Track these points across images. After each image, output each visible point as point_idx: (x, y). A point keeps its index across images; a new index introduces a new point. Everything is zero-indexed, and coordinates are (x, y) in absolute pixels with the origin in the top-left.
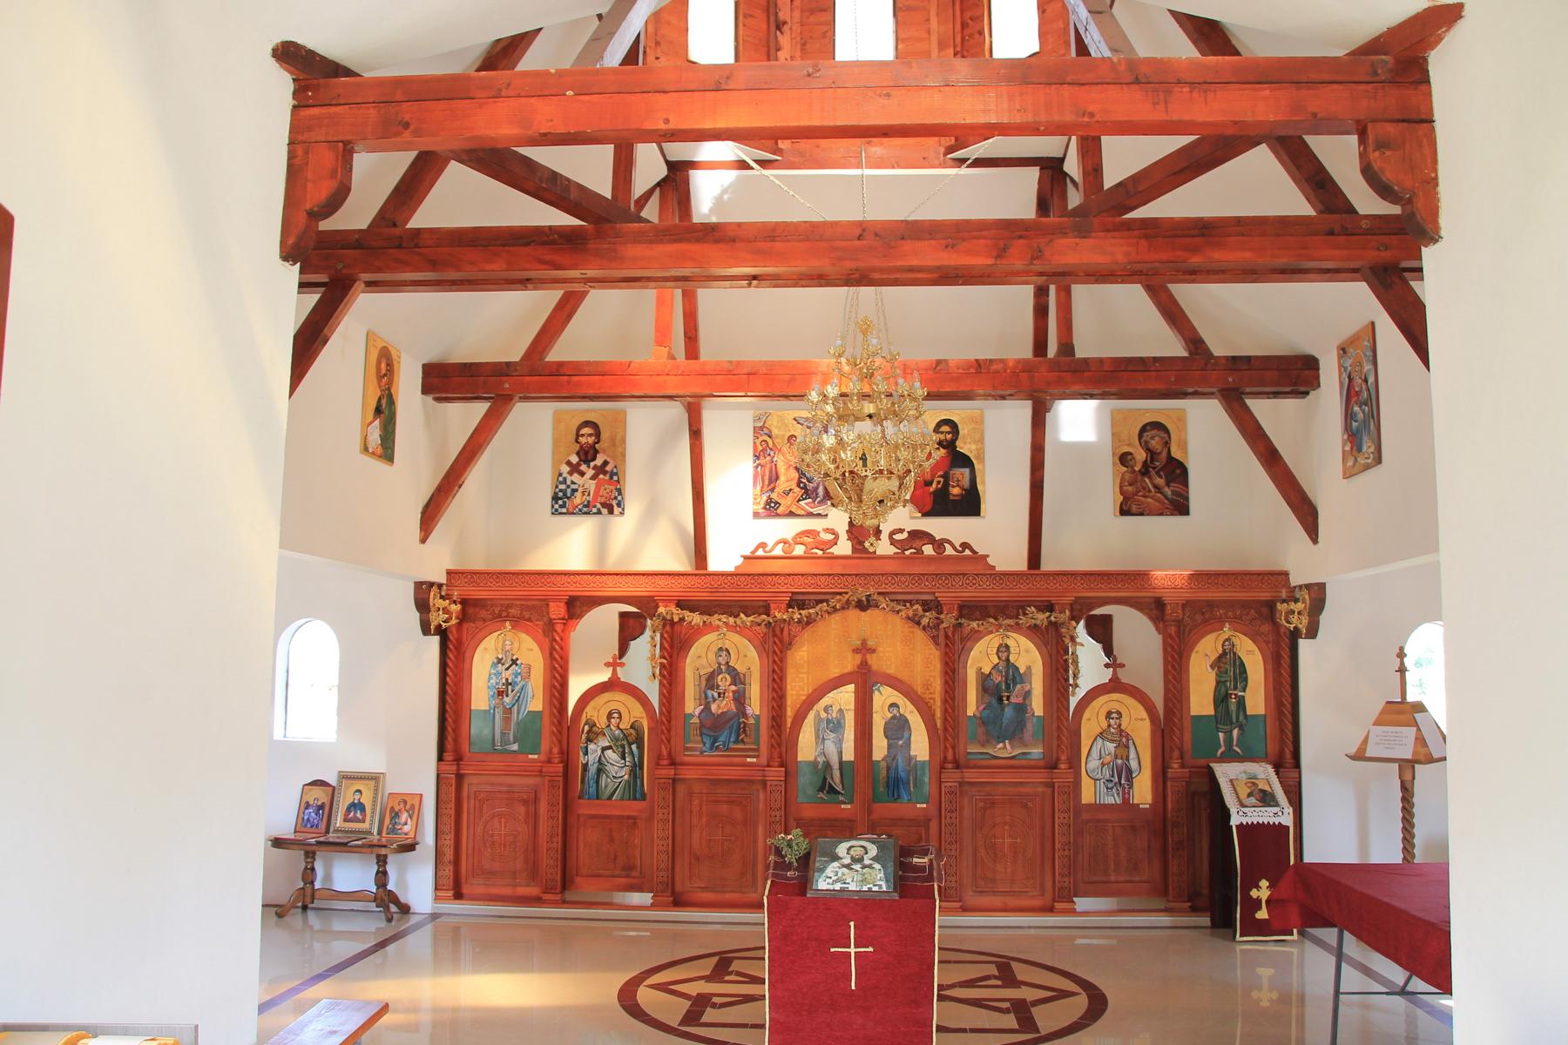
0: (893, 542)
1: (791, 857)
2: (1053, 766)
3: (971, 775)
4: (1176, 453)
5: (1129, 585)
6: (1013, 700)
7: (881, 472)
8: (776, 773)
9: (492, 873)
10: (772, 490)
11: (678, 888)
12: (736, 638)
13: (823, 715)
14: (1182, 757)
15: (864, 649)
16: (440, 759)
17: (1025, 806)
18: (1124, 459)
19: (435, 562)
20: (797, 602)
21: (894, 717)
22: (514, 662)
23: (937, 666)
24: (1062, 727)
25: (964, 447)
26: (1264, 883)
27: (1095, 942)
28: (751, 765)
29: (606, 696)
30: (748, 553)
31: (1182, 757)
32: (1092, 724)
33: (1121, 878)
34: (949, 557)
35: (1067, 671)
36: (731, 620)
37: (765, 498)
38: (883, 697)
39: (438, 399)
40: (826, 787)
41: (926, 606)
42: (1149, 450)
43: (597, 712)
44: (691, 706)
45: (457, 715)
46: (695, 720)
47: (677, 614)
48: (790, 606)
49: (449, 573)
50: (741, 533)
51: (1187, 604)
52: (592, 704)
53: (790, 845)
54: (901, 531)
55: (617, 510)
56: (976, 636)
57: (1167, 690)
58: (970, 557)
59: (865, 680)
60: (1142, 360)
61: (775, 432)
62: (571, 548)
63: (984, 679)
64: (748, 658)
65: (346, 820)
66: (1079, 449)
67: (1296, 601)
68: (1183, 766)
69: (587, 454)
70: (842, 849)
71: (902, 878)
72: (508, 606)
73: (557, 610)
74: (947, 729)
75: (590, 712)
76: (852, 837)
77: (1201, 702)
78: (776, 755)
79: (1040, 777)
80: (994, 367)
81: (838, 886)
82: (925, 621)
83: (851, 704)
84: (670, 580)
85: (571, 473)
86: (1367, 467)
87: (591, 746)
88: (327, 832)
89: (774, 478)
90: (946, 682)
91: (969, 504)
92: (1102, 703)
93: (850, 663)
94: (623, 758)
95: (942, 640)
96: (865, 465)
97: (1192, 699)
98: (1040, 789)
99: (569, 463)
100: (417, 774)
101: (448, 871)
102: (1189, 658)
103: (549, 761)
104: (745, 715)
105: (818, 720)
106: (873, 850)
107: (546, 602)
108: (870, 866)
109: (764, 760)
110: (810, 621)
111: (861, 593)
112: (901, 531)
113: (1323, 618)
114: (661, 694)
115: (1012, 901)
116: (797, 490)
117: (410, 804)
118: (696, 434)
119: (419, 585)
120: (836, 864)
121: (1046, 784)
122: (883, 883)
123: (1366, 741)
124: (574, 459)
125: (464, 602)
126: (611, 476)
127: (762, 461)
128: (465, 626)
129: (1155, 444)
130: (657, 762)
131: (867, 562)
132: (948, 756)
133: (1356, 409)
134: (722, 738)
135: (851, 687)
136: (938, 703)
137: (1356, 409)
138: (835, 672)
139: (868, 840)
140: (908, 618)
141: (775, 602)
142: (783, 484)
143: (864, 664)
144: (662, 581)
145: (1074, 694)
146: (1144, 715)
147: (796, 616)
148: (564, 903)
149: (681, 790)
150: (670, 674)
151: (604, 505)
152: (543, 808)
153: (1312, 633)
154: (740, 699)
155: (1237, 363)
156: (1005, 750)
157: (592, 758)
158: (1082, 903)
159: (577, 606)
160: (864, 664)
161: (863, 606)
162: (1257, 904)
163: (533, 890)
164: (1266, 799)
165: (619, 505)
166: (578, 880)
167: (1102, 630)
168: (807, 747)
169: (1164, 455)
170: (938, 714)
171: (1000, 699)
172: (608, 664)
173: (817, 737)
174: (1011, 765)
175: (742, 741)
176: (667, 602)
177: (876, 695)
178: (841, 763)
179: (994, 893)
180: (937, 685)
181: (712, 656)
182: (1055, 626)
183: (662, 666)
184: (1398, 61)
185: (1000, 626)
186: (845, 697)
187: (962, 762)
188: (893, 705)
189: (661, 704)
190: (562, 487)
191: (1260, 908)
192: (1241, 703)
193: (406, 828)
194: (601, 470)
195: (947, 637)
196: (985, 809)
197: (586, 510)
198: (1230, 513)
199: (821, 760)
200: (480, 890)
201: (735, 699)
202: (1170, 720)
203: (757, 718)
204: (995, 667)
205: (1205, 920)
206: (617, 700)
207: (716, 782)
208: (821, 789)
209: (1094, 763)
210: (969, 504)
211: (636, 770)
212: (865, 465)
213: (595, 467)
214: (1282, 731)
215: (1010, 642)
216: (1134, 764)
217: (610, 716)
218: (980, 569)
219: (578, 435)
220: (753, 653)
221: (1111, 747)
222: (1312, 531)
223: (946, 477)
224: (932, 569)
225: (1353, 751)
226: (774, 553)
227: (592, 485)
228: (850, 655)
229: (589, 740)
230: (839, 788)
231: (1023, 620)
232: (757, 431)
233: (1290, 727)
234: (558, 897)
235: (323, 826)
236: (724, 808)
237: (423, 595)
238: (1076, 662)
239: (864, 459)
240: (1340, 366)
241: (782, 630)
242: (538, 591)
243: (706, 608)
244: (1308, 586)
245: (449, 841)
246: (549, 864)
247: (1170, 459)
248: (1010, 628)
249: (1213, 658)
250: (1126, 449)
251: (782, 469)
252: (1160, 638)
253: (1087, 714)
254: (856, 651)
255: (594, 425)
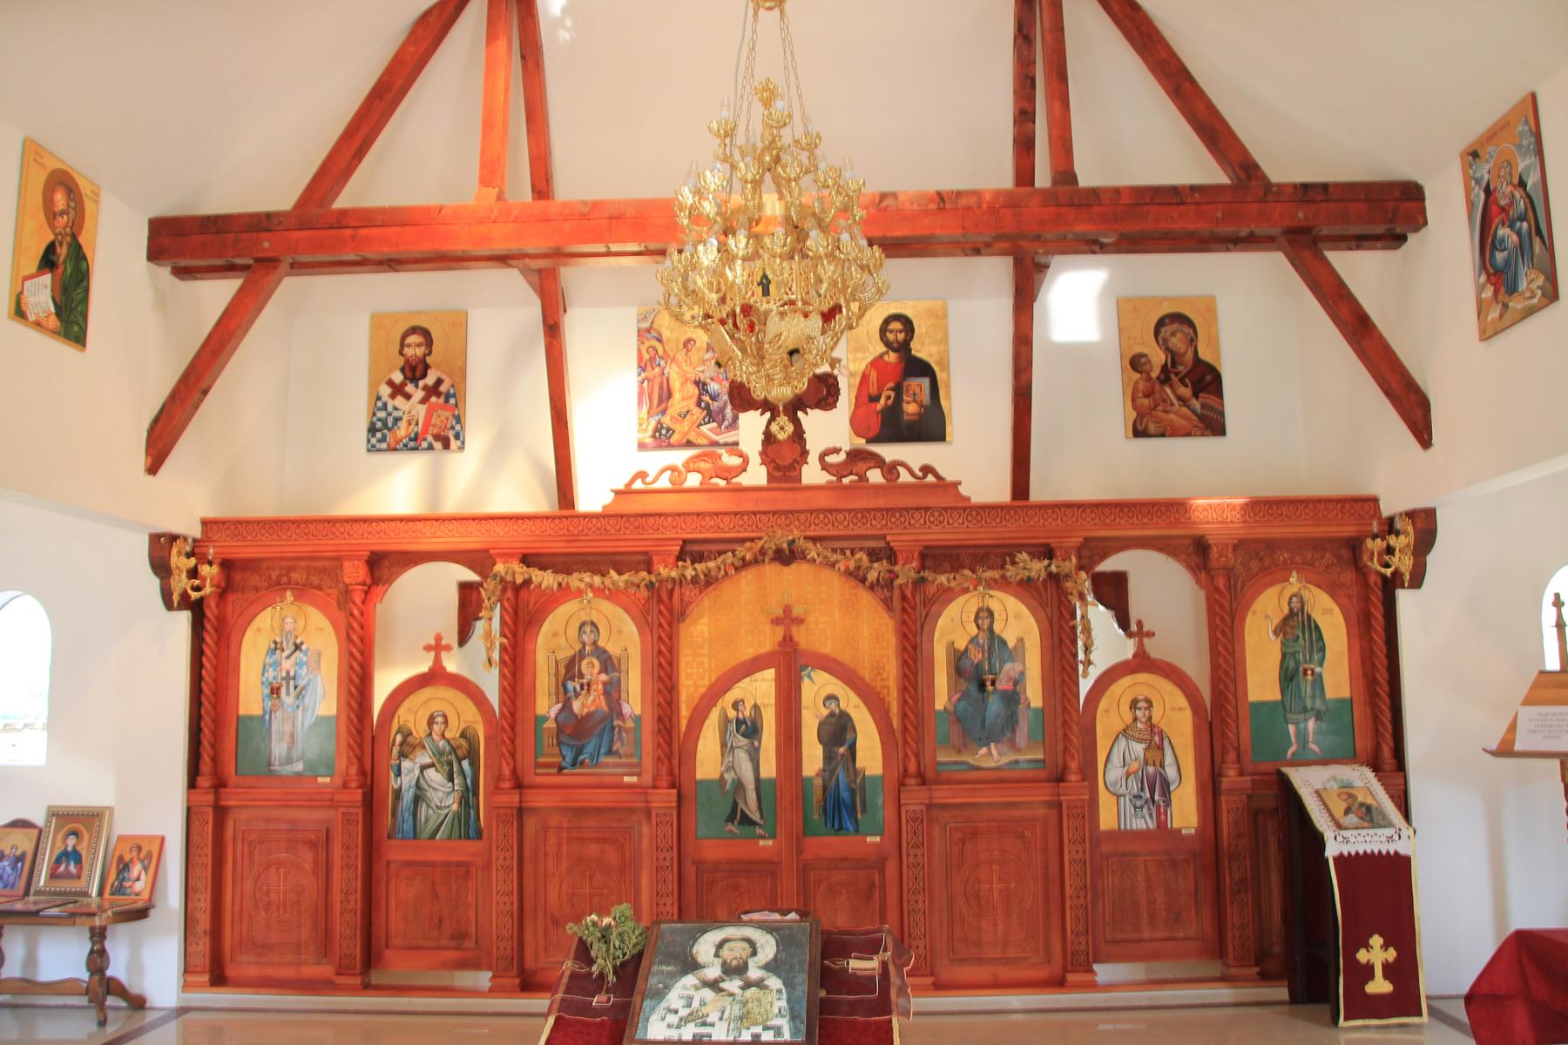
0: (825, 467)
1: (603, 964)
2: (1060, 778)
3: (942, 795)
4: (1205, 354)
5: (1160, 522)
6: (998, 685)
7: (793, 303)
8: (664, 798)
9: (266, 947)
10: (664, 412)
11: (530, 963)
12: (607, 607)
13: (732, 714)
14: (1239, 760)
15: (787, 619)
16: (192, 784)
17: (1021, 836)
18: (1136, 363)
19: (184, 500)
20: (690, 552)
21: (832, 714)
22: (297, 647)
23: (890, 641)
24: (1070, 725)
25: (921, 349)
26: (1376, 941)
27: (1126, 1027)
28: (630, 786)
29: (427, 693)
30: (621, 487)
31: (1239, 761)
32: (1110, 718)
33: (1158, 935)
34: (905, 486)
35: (1074, 642)
36: (597, 580)
37: (653, 423)
38: (817, 687)
39: (182, 272)
40: (737, 816)
41: (874, 555)
42: (1168, 350)
43: (412, 715)
44: (546, 706)
45: (218, 722)
46: (551, 724)
47: (520, 572)
48: (680, 557)
49: (205, 523)
50: (617, 455)
51: (1240, 545)
52: (406, 704)
53: (605, 938)
54: (836, 451)
55: (454, 444)
56: (946, 595)
57: (1215, 668)
58: (937, 486)
59: (790, 663)
60: (1174, 190)
61: (666, 334)
62: (396, 489)
63: (958, 660)
64: (624, 635)
65: (53, 875)
66: (1076, 353)
67: (1397, 534)
68: (1241, 773)
69: (415, 371)
70: (704, 947)
71: (825, 1006)
72: (290, 569)
73: (355, 572)
74: (908, 726)
75: (404, 715)
76: (719, 923)
77: (1262, 684)
78: (664, 771)
79: (1042, 794)
80: (964, 201)
81: (688, 1033)
82: (872, 576)
83: (776, 682)
84: (514, 527)
85: (393, 396)
86: (1530, 312)
87: (406, 764)
88: (27, 893)
89: (666, 395)
90: (905, 662)
91: (930, 427)
92: (1123, 688)
93: (767, 640)
94: (451, 779)
95: (897, 603)
96: (766, 292)
97: (1250, 678)
98: (1041, 812)
99: (390, 383)
100: (156, 807)
101: (203, 946)
102: (1243, 620)
103: (345, 786)
104: (621, 715)
105: (725, 721)
106: (768, 947)
107: (338, 559)
108: (759, 984)
109: (648, 779)
110: (709, 581)
111: (782, 539)
112: (836, 451)
113: (1431, 559)
114: (503, 689)
115: (1006, 973)
116: (696, 411)
117: (148, 851)
118: (553, 331)
119: (155, 539)
120: (690, 980)
121: (1050, 805)
122: (784, 1023)
123: (1513, 728)
124: (398, 377)
125: (227, 565)
126: (446, 397)
127: (649, 373)
128: (232, 597)
129: (1177, 342)
130: (495, 789)
131: (790, 495)
132: (911, 766)
133: (1503, 232)
134: (589, 749)
135: (770, 673)
136: (894, 693)
137: (1503, 232)
138: (748, 652)
139: (761, 925)
140: (849, 574)
141: (658, 553)
142: (677, 404)
143: (788, 640)
144: (499, 529)
145: (1085, 674)
146: (1183, 702)
147: (689, 573)
148: (367, 987)
149: (531, 825)
150: (515, 662)
151: (437, 437)
152: (337, 853)
153: (1417, 580)
154: (613, 692)
155: (1308, 192)
156: (992, 757)
157: (407, 781)
158: (1104, 972)
159: (384, 565)
160: (788, 640)
161: (786, 557)
162: (1368, 972)
163: (325, 970)
164: (1369, 816)
165: (457, 437)
166: (388, 953)
167: (1113, 591)
168: (708, 760)
169: (1190, 356)
170: (894, 708)
171: (982, 686)
172: (428, 648)
173: (723, 744)
174: (998, 779)
175: (617, 753)
176: (507, 557)
177: (806, 685)
178: (758, 780)
179: (979, 961)
180: (892, 669)
181: (573, 632)
182: (1054, 579)
183: (503, 648)
184: (978, 667)
185: (978, 582)
186: (761, 689)
187: (930, 775)
188: (831, 698)
189: (502, 703)
190: (382, 414)
191: (1371, 976)
192: (1318, 681)
193: (139, 886)
194: (433, 390)
195: (904, 598)
196: (963, 841)
197: (414, 443)
198: (1292, 417)
199: (729, 777)
200: (251, 972)
201: (606, 693)
202: (1219, 713)
203: (638, 720)
204: (973, 640)
205: (1282, 993)
206: (439, 698)
207: (580, 812)
208: (731, 819)
209: (1115, 773)
210: (930, 427)
211: (468, 797)
212: (766, 292)
213: (425, 388)
214: (1376, 720)
215: (994, 605)
216: (1171, 772)
217: (431, 721)
218: (948, 501)
219: (402, 345)
220: (630, 628)
221: (1139, 749)
222: (1422, 432)
223: (898, 389)
224: (881, 502)
225: (1494, 746)
226: (659, 485)
227: (421, 412)
228: (768, 627)
229: (403, 755)
230: (756, 817)
231: (1011, 571)
232: (642, 334)
233: (1388, 714)
234: (358, 981)
235: (21, 884)
236: (593, 849)
237: (161, 548)
238: (1087, 630)
239: (765, 284)
240: (1467, 180)
241: (671, 593)
242: (326, 545)
243: (564, 564)
244: (1411, 515)
245: (203, 902)
246: (346, 928)
247: (1198, 362)
248: (992, 584)
249: (1277, 620)
250: (1138, 349)
251: (676, 384)
252: (1202, 594)
253: (1103, 704)
254: (776, 622)
255: (426, 333)
